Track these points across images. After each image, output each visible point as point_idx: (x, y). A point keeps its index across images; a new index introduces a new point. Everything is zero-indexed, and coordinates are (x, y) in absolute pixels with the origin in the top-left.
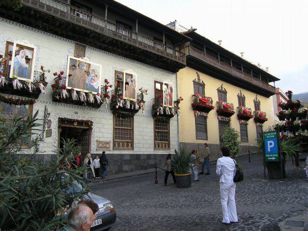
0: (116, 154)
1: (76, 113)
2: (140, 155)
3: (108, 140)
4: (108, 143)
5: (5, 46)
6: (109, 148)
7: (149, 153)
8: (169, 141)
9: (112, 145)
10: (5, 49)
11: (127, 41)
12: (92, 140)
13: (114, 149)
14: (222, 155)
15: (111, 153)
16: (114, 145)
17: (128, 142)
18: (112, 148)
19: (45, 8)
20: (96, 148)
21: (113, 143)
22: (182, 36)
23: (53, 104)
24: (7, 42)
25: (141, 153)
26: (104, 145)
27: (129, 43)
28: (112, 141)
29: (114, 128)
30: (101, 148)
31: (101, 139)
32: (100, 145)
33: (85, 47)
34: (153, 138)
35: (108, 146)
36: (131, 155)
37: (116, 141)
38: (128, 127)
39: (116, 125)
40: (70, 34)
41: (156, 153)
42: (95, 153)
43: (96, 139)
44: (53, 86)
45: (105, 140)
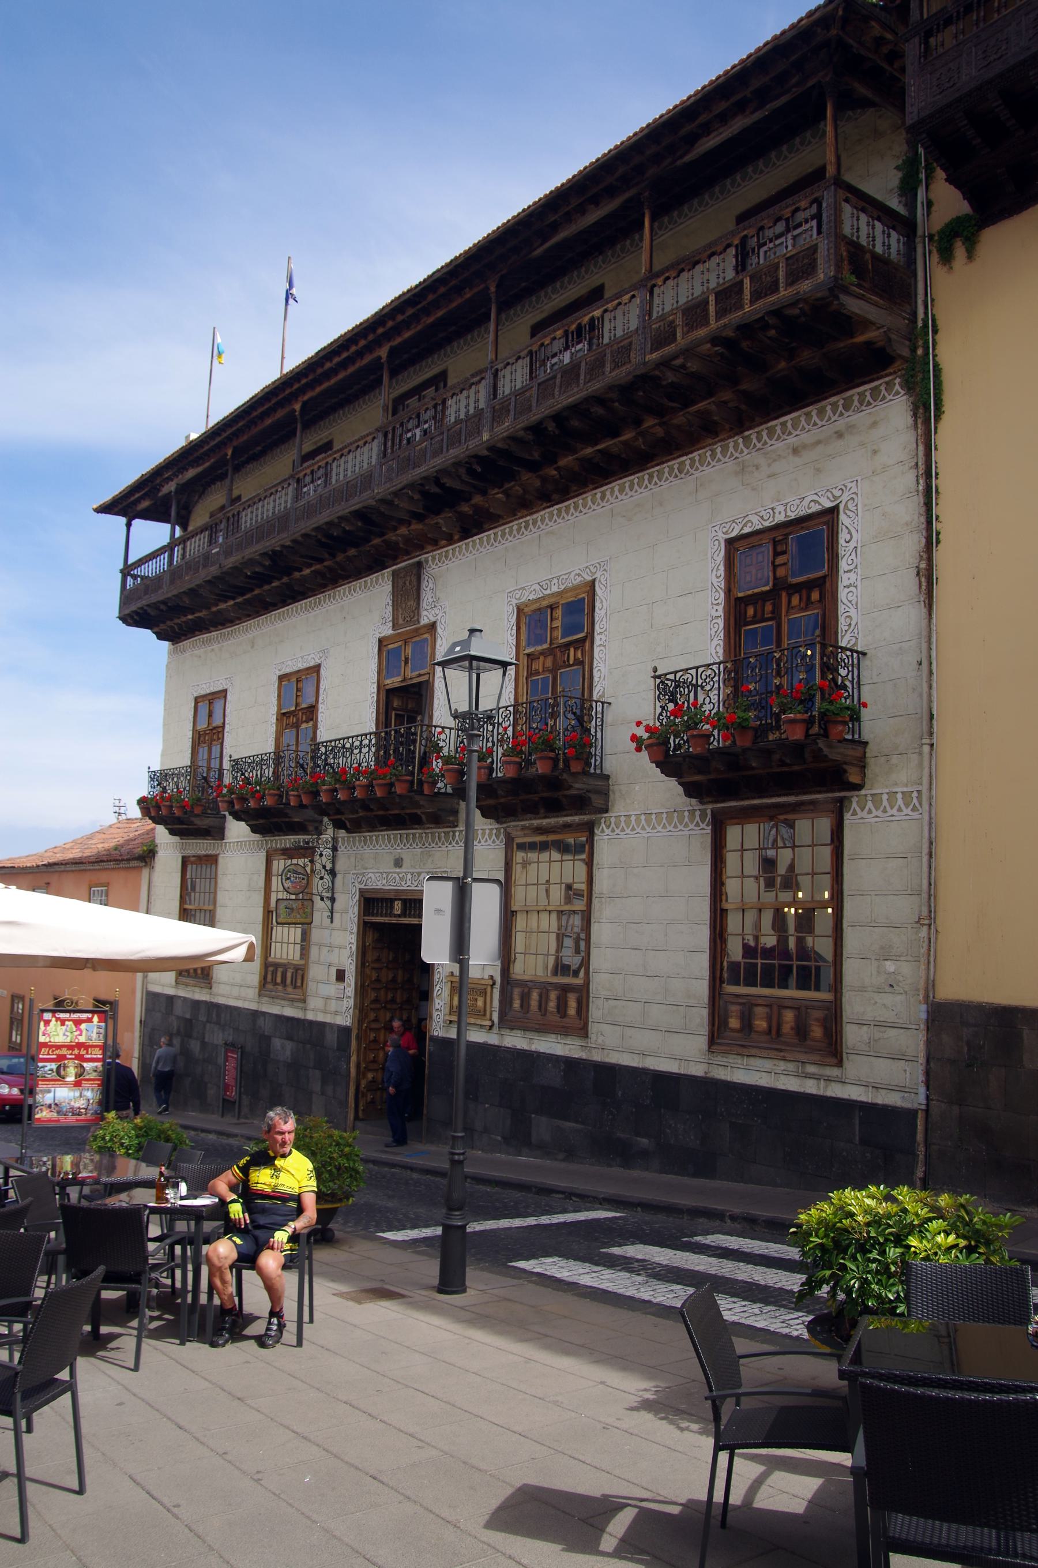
36: (571, 1065)
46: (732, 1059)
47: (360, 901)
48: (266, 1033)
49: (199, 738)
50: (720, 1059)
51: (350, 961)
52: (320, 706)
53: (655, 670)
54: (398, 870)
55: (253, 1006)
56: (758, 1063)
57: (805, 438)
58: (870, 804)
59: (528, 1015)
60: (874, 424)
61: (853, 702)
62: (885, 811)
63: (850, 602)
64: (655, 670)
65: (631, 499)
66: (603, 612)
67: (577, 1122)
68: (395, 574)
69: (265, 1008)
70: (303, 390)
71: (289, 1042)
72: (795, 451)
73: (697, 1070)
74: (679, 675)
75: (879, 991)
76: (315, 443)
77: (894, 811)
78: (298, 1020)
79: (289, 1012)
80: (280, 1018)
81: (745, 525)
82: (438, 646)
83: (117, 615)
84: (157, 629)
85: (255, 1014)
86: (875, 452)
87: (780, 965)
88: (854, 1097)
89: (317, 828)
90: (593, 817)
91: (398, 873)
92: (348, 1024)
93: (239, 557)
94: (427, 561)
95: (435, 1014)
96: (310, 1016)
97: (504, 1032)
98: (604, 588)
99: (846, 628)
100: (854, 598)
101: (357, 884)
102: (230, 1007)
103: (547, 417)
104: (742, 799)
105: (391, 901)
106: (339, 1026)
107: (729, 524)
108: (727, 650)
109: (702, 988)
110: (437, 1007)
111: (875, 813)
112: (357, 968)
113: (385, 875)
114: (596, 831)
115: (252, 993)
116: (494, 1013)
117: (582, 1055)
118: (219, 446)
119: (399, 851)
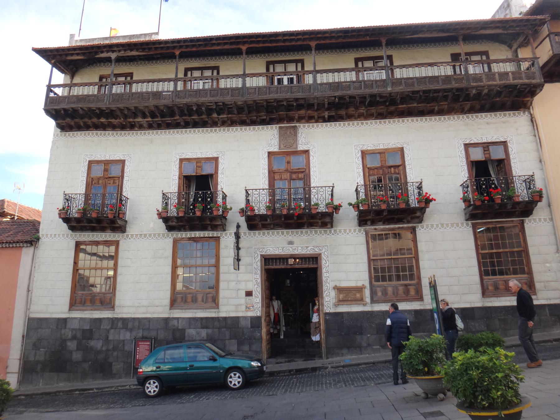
0: (357, 312)
1: (291, 243)
2: (238, 318)
3: (360, 284)
4: (360, 289)
5: (463, 152)
7: (468, 306)
8: (530, 273)
10: (178, 170)
11: (485, 82)
12: (325, 288)
15: (368, 308)
16: (373, 293)
17: (406, 285)
18: (368, 300)
19: (453, 82)
22: (528, 20)
24: (180, 159)
27: (359, 92)
28: (367, 284)
34: (475, 270)
40: (264, 116)
41: (172, 316)
42: (332, 311)
43: (332, 284)
46: (492, 299)
47: (261, 260)
48: (180, 328)
49: (92, 182)
50: (488, 299)
51: (256, 286)
52: (220, 176)
53: (64, 192)
55: (166, 316)
56: (503, 298)
57: (490, 120)
58: (532, 221)
59: (387, 297)
60: (515, 122)
62: (538, 223)
64: (64, 192)
67: (424, 332)
68: (280, 127)
70: (252, 42)
71: (206, 330)
72: (488, 123)
73: (480, 305)
74: (73, 195)
75: (545, 272)
76: (205, 64)
77: (541, 223)
79: (213, 315)
81: (471, 140)
83: (43, 107)
84: (60, 121)
85: (167, 320)
86: (517, 129)
88: (543, 303)
89: (223, 228)
90: (414, 225)
92: (258, 315)
93: (190, 100)
94: (300, 127)
97: (373, 305)
102: (139, 318)
103: (422, 90)
104: (484, 220)
105: (287, 259)
109: (477, 278)
111: (535, 224)
112: (262, 289)
117: (422, 308)
118: (174, 48)
119: (290, 238)
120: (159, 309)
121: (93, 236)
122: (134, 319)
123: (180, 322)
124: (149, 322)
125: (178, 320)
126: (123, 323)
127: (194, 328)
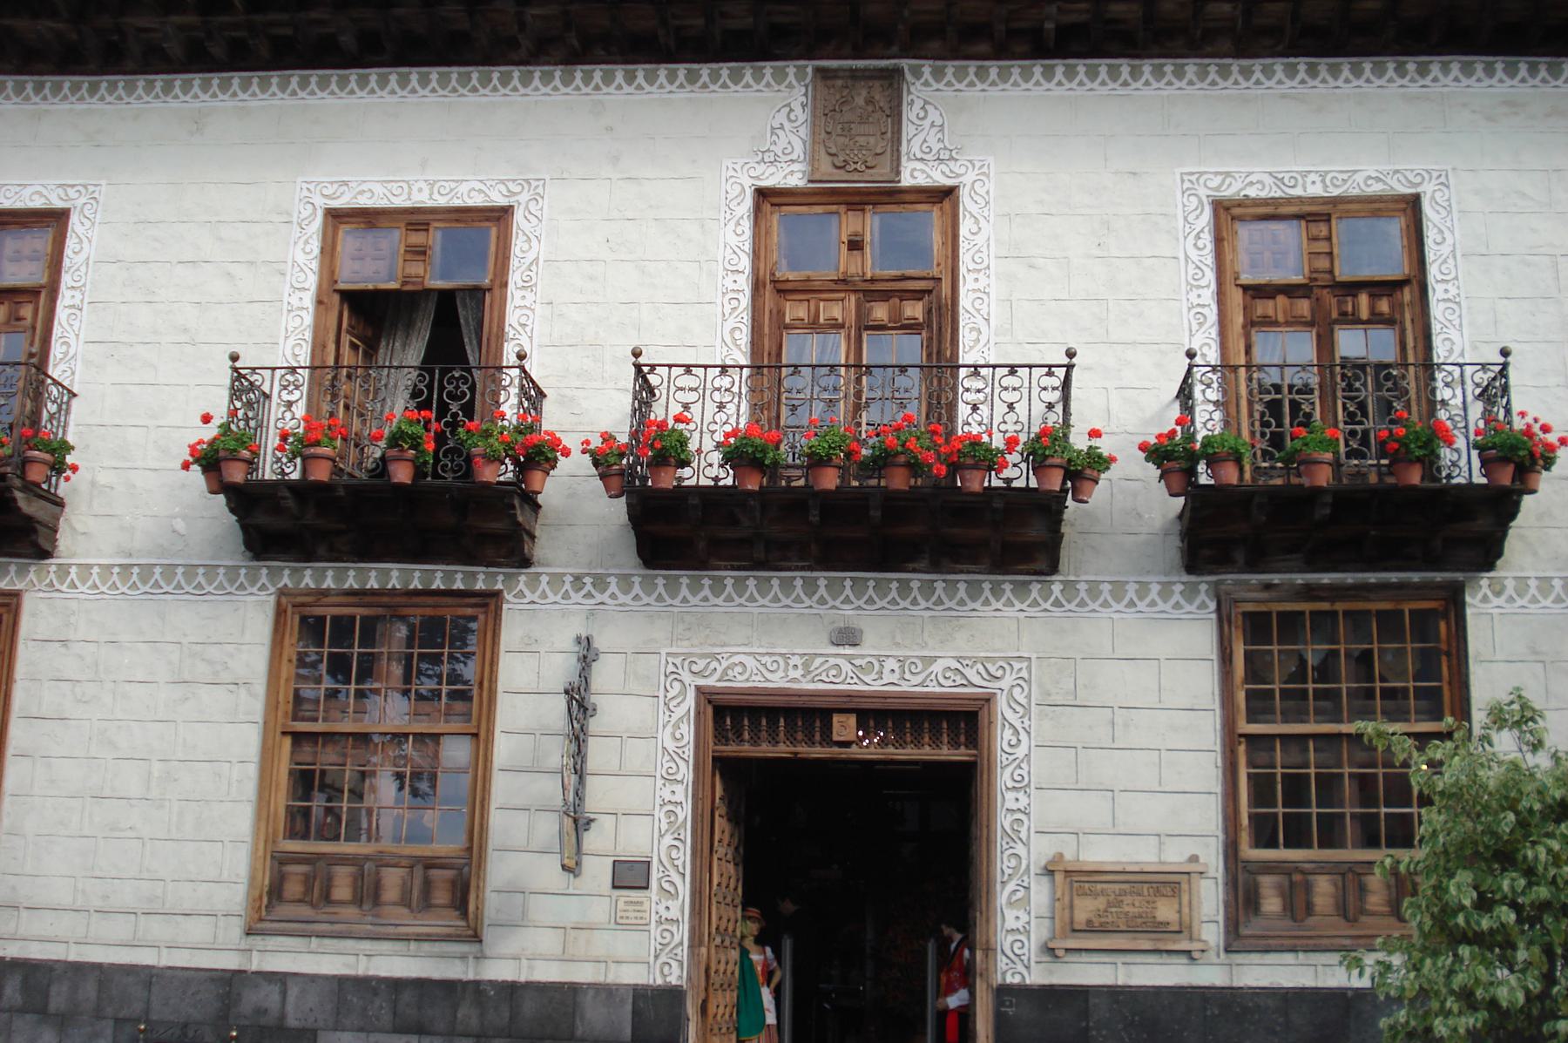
0: (1158, 991)
1: (847, 637)
2: (571, 991)
3: (1174, 856)
4: (1169, 883)
6: (1184, 929)
9: (1210, 899)
13: (1235, 940)
14: (588, 1000)
15: (1209, 975)
18: (1212, 934)
20: (1039, 933)
21: (1232, 882)
23: (649, 586)
25: (583, 974)
26: (1132, 906)
28: (1212, 858)
29: (1231, 738)
30: (1090, 929)
31: (1100, 853)
32: (1085, 909)
33: (892, 79)
35: (1165, 911)
37: (1269, 868)
38: (1301, 717)
39: (1259, 706)
42: (1037, 976)
43: (1040, 850)
44: (312, 368)
45: (1142, 855)
48: (292, 1022)
54: (848, 651)
55: (229, 962)
61: (1239, 434)
63: (978, 311)
65: (1490, 90)
66: (1446, 250)
69: (257, 963)
78: (449, 987)
80: (342, 984)
81: (362, 192)
82: (68, 252)
85: (230, 983)
87: (1378, 806)
90: (1459, 576)
91: (849, 658)
92: (673, 980)
95: (1004, 941)
96: (499, 970)
98: (1444, 213)
99: (972, 344)
100: (985, 307)
101: (687, 677)
102: (98, 967)
106: (326, 978)
107: (335, 186)
108: (502, 345)
110: (1011, 923)
113: (796, 660)
114: (1468, 599)
115: (233, 930)
116: (352, 959)
119: (847, 614)
120: (198, 930)
121: (361, 573)
122: (79, 970)
123: (293, 992)
124: (149, 985)
125: (284, 984)
126: (26, 987)
127: (361, 1030)
